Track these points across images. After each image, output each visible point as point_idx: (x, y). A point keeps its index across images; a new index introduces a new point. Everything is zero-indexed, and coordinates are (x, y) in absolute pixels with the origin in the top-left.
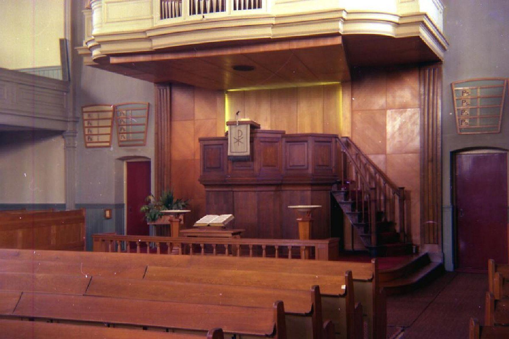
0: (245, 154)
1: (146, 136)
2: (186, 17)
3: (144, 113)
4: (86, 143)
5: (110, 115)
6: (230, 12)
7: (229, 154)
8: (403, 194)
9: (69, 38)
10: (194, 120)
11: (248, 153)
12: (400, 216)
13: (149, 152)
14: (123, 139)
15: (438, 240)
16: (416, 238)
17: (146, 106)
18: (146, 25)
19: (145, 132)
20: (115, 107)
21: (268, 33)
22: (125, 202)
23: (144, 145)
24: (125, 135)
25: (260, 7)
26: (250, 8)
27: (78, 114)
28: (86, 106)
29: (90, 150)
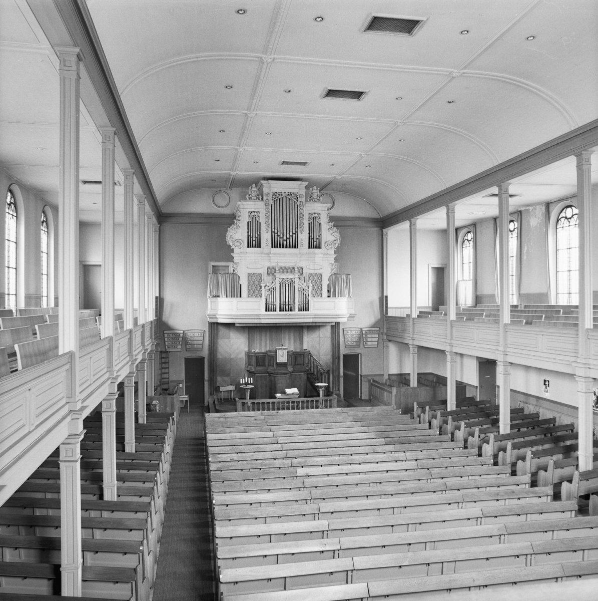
6: (297, 312)
17: (203, 332)
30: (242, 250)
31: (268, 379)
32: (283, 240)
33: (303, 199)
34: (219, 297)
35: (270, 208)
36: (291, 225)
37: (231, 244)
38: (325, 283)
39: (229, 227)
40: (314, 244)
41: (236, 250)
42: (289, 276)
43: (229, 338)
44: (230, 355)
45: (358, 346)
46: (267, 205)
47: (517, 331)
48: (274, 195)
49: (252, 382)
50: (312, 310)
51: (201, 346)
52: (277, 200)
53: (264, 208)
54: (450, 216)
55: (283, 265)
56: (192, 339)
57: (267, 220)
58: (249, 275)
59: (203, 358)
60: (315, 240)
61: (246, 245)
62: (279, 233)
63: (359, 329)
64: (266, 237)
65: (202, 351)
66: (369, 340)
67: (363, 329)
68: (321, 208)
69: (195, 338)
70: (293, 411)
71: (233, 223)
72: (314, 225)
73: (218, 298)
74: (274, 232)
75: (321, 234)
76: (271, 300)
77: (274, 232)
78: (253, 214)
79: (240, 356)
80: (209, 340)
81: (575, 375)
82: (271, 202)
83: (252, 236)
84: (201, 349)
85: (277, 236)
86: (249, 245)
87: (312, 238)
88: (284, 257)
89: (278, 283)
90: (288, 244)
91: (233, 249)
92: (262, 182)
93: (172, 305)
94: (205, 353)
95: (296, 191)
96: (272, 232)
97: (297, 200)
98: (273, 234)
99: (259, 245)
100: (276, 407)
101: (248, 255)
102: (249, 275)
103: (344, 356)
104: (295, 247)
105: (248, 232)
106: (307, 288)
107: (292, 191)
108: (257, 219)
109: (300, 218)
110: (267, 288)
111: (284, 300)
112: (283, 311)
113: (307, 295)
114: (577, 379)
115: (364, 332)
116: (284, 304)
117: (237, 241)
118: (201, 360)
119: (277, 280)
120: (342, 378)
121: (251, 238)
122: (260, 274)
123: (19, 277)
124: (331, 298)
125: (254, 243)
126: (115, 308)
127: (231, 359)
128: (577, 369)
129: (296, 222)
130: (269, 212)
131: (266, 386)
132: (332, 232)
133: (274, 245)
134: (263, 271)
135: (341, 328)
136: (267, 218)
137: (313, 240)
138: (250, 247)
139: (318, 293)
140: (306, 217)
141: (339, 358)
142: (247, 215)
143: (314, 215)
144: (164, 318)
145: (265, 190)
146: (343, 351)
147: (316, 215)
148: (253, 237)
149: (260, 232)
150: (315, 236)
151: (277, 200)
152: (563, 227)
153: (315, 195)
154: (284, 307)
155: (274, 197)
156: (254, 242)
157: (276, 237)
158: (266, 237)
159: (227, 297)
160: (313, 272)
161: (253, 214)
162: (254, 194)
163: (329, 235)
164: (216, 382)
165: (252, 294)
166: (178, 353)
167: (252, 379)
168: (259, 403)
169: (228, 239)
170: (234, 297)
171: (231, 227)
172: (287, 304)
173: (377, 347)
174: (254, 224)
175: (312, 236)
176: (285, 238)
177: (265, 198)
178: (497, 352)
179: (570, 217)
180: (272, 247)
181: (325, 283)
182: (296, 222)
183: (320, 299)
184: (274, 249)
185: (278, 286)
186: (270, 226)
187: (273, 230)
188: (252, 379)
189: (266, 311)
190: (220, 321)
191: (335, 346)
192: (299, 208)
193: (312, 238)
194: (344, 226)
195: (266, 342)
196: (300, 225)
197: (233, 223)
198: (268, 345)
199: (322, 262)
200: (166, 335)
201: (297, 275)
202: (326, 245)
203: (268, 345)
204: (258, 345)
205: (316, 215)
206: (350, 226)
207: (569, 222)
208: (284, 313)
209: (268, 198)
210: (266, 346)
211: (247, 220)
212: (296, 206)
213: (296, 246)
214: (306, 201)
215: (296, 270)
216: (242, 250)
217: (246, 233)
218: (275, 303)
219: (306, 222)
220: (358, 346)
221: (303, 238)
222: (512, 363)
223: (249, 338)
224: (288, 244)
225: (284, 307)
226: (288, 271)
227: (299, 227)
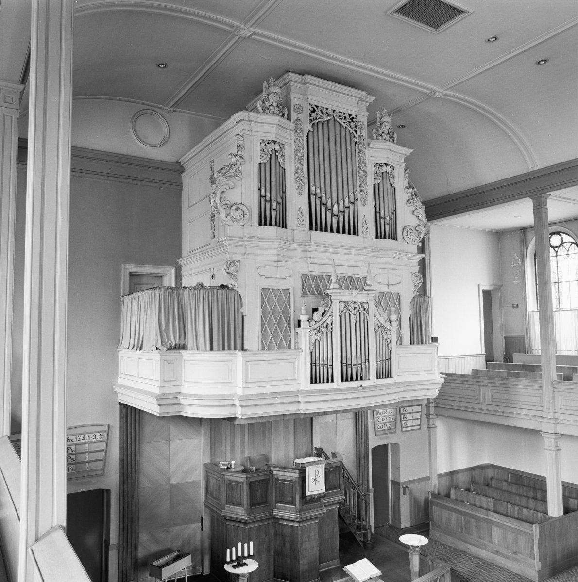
1: (104, 465)
17: (106, 428)
30: (247, 231)
31: (272, 531)
34: (184, 347)
36: (345, 180)
44: (169, 479)
45: (394, 431)
48: (314, 111)
49: (251, 553)
51: (100, 465)
53: (293, 138)
54: (539, 210)
55: (343, 271)
56: (81, 449)
57: (299, 165)
58: (264, 291)
64: (297, 204)
65: (103, 475)
66: (409, 417)
69: (86, 448)
72: (382, 190)
73: (182, 351)
76: (321, 355)
78: (273, 146)
79: (191, 479)
80: (121, 448)
81: (541, 431)
82: (307, 127)
83: (268, 199)
84: (102, 472)
86: (263, 221)
88: (334, 254)
92: (292, 76)
94: (111, 481)
98: (313, 198)
99: (282, 223)
102: (264, 291)
105: (260, 189)
111: (349, 355)
112: (352, 380)
114: (543, 435)
116: (349, 363)
118: (101, 495)
121: (268, 205)
122: (286, 291)
127: (174, 486)
128: (543, 424)
131: (268, 550)
132: (413, 208)
133: (315, 225)
134: (294, 285)
136: (299, 160)
137: (382, 221)
138: (265, 225)
140: (370, 170)
145: (296, 99)
146: (373, 442)
148: (270, 201)
152: (568, 254)
153: (386, 128)
154: (349, 370)
155: (314, 115)
156: (274, 214)
158: (297, 204)
159: (212, 349)
160: (385, 289)
162: (273, 100)
164: (136, 547)
165: (271, 342)
167: (251, 543)
170: (229, 349)
172: (354, 362)
173: (420, 429)
174: (271, 171)
175: (382, 212)
177: (294, 116)
178: (540, 420)
179: (558, 245)
180: (311, 229)
188: (251, 543)
190: (191, 412)
193: (382, 215)
198: (247, 447)
202: (405, 233)
203: (247, 447)
204: (228, 448)
205: (388, 169)
207: (557, 252)
209: (301, 117)
210: (242, 451)
211: (257, 160)
214: (370, 137)
216: (247, 231)
218: (330, 363)
219: (370, 181)
220: (393, 430)
221: (366, 213)
222: (562, 434)
223: (211, 435)
225: (349, 370)
226: (349, 287)
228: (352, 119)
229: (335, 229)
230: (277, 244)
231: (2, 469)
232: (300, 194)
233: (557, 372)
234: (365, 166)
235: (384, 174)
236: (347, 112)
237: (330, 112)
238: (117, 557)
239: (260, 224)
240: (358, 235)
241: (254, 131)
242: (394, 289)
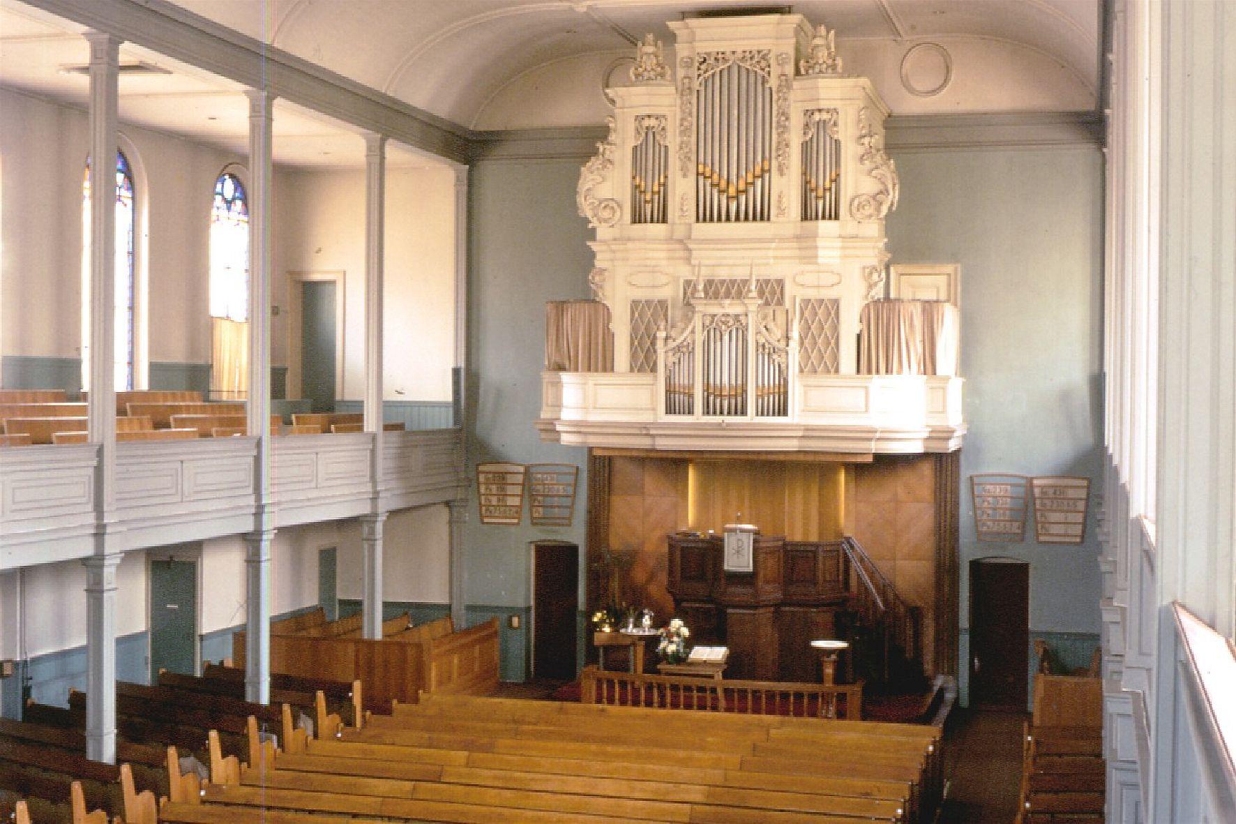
0: (746, 570)
1: (571, 513)
2: (699, 417)
3: (571, 479)
4: (482, 517)
5: (520, 478)
6: (751, 417)
7: (726, 568)
8: (915, 614)
9: (462, 364)
10: (643, 493)
11: (751, 569)
12: (778, 425)
13: (576, 535)
14: (536, 515)
15: (953, 672)
16: (928, 667)
17: (574, 471)
18: (646, 418)
19: (571, 507)
20: (527, 469)
21: (792, 445)
22: (532, 603)
23: (569, 525)
24: (541, 509)
25: (785, 413)
26: (774, 414)
27: (472, 475)
28: (484, 463)
29: (486, 527)
32: (728, 198)
33: (790, 69)
35: (694, 101)
37: (589, 214)
38: (850, 326)
39: (584, 163)
40: (817, 205)
41: (603, 232)
42: (731, 307)
43: (641, 491)
46: (684, 91)
47: (67, 465)
50: (796, 415)
52: (713, 75)
53: (679, 102)
58: (635, 304)
59: (573, 549)
60: (820, 193)
61: (628, 216)
62: (716, 177)
63: (1023, 482)
67: (1035, 482)
68: (839, 95)
70: (648, 710)
71: (595, 152)
72: (818, 149)
74: (703, 174)
75: (838, 175)
76: (681, 380)
77: (703, 174)
85: (712, 185)
86: (637, 218)
87: (813, 185)
89: (699, 328)
90: (743, 208)
91: (594, 229)
93: (499, 393)
95: (764, 45)
96: (698, 174)
97: (769, 73)
100: (695, 701)
101: (630, 245)
102: (635, 304)
103: (975, 565)
104: (762, 219)
105: (634, 178)
106: (782, 344)
107: (753, 45)
108: (658, 137)
109: (779, 125)
110: (672, 344)
112: (715, 413)
113: (783, 366)
115: (1037, 491)
117: (609, 204)
119: (697, 322)
120: (967, 637)
123: (1092, 328)
124: (864, 375)
125: (648, 208)
126: (385, 399)
129: (767, 137)
130: (690, 114)
133: (705, 215)
135: (965, 473)
136: (684, 132)
139: (823, 361)
140: (796, 121)
141: (954, 569)
142: (631, 126)
143: (817, 117)
144: (481, 427)
146: (969, 550)
147: (825, 116)
149: (666, 177)
150: (821, 182)
151: (713, 75)
155: (703, 67)
157: (708, 188)
158: (682, 189)
160: (812, 294)
161: (646, 123)
163: (861, 177)
166: (513, 529)
168: (745, 691)
169: (580, 199)
171: (589, 164)
175: (813, 181)
176: (732, 191)
181: (850, 326)
182: (767, 137)
183: (831, 380)
184: (701, 225)
185: (700, 337)
186: (694, 158)
187: (701, 170)
189: (670, 410)
191: (946, 530)
192: (775, 97)
193: (813, 185)
194: (978, 144)
195: (806, 503)
196: (778, 149)
197: (595, 152)
199: (842, 263)
200: (482, 478)
201: (753, 304)
206: (997, 144)
208: (717, 419)
211: (631, 142)
212: (767, 92)
213: (762, 215)
215: (753, 288)
217: (629, 179)
219: (795, 139)
221: (786, 189)
224: (743, 208)
227: (774, 154)
228: (764, 58)
229: (742, 216)
230: (840, 244)
231: (1231, 656)
232: (685, 176)
233: (607, 366)
234: (787, 119)
235: (819, 129)
236: (755, 49)
237: (728, 54)
238: (447, 576)
239: (634, 222)
240: (769, 219)
241: (643, 102)
242: (828, 294)
